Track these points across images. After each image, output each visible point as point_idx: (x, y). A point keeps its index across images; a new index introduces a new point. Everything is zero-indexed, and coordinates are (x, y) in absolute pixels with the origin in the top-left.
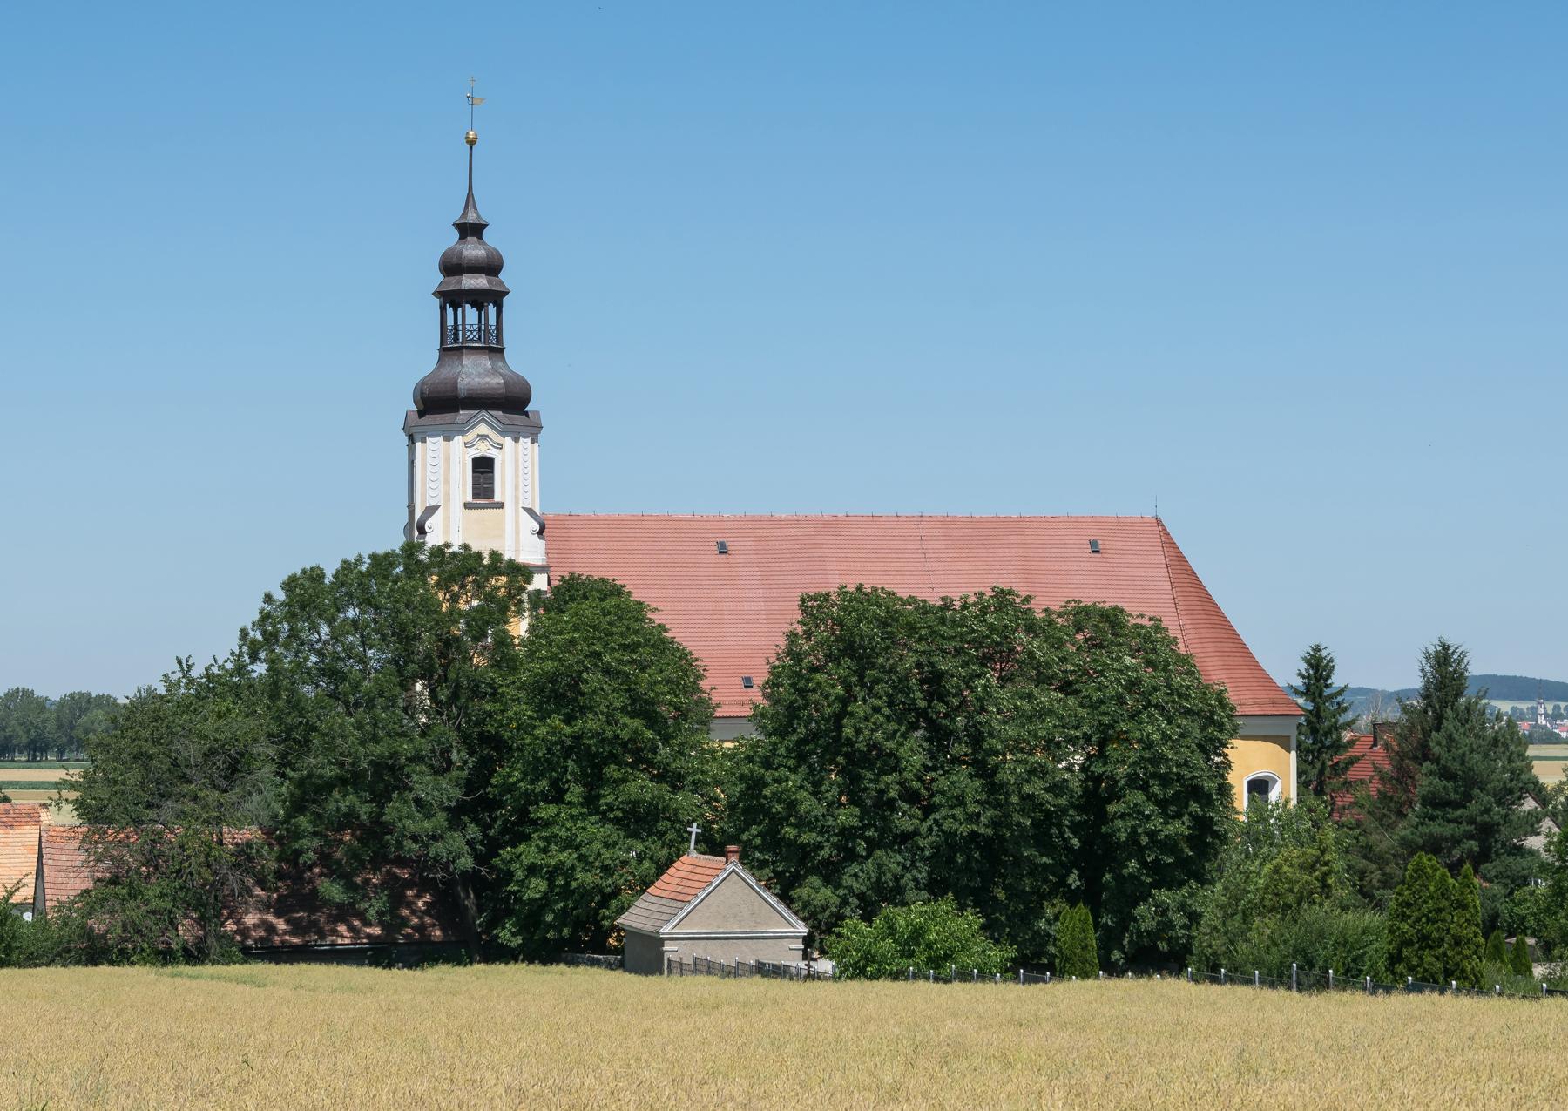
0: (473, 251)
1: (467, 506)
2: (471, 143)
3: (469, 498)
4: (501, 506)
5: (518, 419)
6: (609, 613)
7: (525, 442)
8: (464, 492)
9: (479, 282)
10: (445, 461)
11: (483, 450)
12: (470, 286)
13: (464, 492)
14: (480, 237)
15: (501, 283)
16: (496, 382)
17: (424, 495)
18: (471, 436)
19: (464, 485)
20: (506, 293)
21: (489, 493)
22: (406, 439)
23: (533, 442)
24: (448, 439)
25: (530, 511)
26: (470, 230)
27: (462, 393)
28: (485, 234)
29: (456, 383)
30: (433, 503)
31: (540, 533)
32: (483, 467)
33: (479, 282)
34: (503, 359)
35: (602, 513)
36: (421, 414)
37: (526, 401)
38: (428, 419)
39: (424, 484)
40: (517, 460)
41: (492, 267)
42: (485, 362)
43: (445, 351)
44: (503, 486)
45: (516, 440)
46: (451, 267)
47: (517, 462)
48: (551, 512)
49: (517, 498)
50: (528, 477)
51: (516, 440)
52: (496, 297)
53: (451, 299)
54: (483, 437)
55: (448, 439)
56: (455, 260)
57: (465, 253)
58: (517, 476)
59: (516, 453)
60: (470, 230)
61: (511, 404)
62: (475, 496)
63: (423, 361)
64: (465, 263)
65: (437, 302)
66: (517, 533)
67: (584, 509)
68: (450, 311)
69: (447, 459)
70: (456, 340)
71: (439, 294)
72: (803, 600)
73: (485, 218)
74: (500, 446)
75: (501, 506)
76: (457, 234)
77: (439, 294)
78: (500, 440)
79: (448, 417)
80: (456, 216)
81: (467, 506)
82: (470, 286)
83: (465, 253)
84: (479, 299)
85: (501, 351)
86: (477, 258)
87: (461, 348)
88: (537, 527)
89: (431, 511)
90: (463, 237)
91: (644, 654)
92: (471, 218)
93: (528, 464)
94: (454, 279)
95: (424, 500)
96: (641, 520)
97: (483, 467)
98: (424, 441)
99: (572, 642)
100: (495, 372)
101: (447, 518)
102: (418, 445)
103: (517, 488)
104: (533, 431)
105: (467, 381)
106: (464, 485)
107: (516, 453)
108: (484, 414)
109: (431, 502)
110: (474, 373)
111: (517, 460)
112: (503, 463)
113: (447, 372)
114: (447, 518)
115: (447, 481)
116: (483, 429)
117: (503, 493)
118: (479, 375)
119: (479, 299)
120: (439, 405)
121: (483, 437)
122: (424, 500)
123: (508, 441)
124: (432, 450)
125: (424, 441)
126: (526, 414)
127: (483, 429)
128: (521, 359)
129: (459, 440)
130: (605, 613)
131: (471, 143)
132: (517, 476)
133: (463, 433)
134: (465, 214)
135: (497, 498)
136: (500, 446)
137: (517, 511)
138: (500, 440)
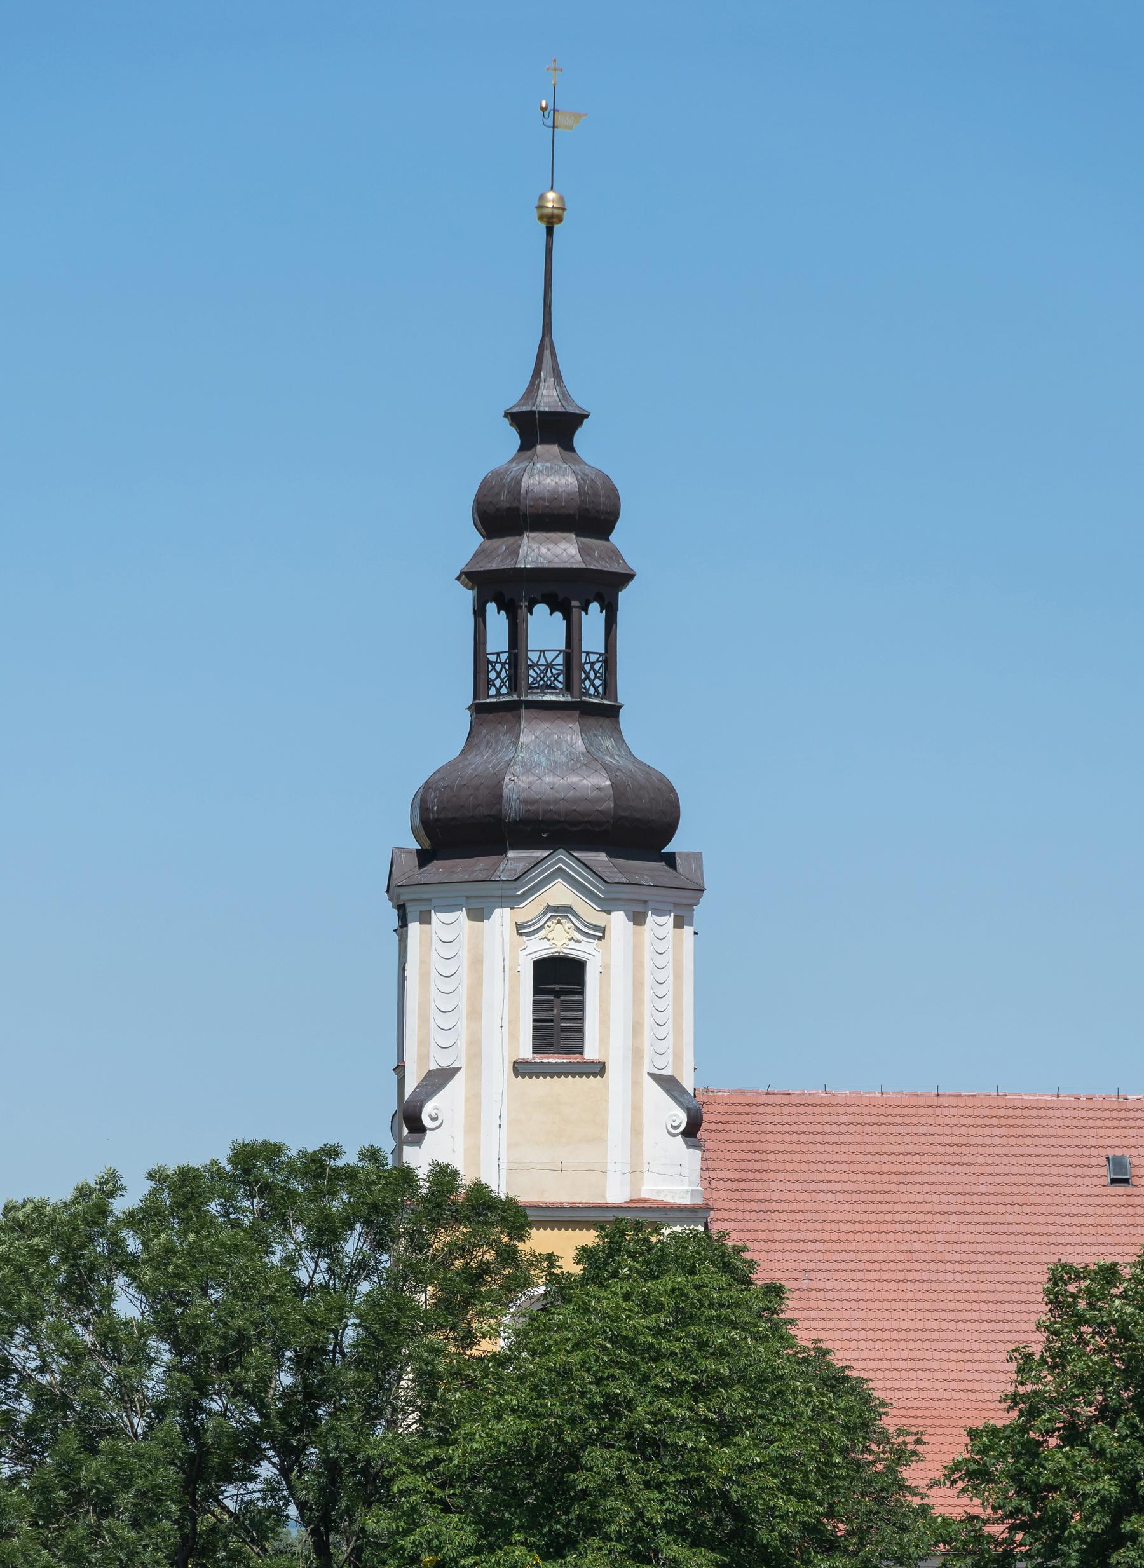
0: (549, 477)
1: (521, 1069)
2: (551, 221)
3: (526, 1052)
4: (598, 1069)
5: (646, 870)
6: (660, 1307)
7: (659, 925)
8: (514, 1036)
9: (559, 551)
10: (472, 966)
11: (558, 940)
12: (545, 560)
13: (514, 1036)
14: (567, 445)
15: (616, 554)
16: (593, 783)
17: (424, 1043)
18: (531, 909)
19: (514, 1022)
20: (627, 578)
21: (573, 1042)
22: (392, 917)
23: (679, 923)
24: (478, 915)
25: (669, 1084)
26: (547, 428)
27: (512, 810)
28: (580, 438)
29: (499, 785)
30: (446, 1062)
31: (691, 1132)
32: (559, 979)
33: (559, 551)
34: (617, 729)
35: (843, 1091)
36: (424, 857)
37: (669, 829)
38: (438, 869)
39: (424, 1020)
40: (638, 965)
41: (593, 516)
42: (571, 737)
43: (483, 711)
44: (607, 1017)
45: (638, 919)
46: (500, 515)
47: (637, 968)
48: (726, 1082)
49: (637, 1054)
50: (667, 1004)
51: (638, 919)
52: (604, 587)
53: (500, 589)
54: (559, 912)
55: (478, 915)
56: (504, 500)
57: (527, 482)
58: (638, 1001)
59: (637, 949)
60: (547, 428)
61: (632, 836)
62: (541, 1044)
63: (434, 734)
64: (526, 505)
65: (468, 596)
66: (637, 1132)
67: (801, 1078)
68: (497, 621)
69: (477, 962)
70: (514, 687)
71: (471, 578)
72: (1055, 1280)
73: (581, 400)
74: (600, 933)
75: (598, 1069)
76: (513, 438)
77: (471, 578)
78: (599, 919)
79: (480, 865)
80: (512, 397)
81: (521, 1069)
82: (545, 560)
83: (527, 482)
84: (568, 591)
85: (612, 712)
86: (555, 496)
87: (512, 708)
88: (682, 1118)
89: (438, 1079)
90: (527, 445)
91: (733, 1402)
92: (548, 399)
93: (668, 974)
94: (501, 544)
95: (423, 1057)
96: (931, 1108)
97: (559, 979)
98: (425, 919)
99: (565, 1374)
100: (592, 760)
101: (474, 1099)
102: (414, 928)
103: (637, 1029)
104: (682, 898)
105: (523, 781)
106: (514, 1022)
107: (637, 949)
108: (562, 859)
109: (439, 1060)
110: (547, 764)
111: (638, 965)
112: (605, 972)
113: (483, 761)
114: (474, 1099)
115: (475, 1013)
116: (559, 893)
117: (604, 1040)
118: (554, 768)
119: (568, 591)
120: (466, 837)
121: (559, 912)
122: (423, 1057)
123: (618, 921)
124: (444, 933)
125: (425, 919)
126: (671, 860)
127: (559, 893)
128: (656, 732)
129: (502, 918)
130: (649, 1306)
131: (551, 221)
132: (638, 1001)
133: (513, 901)
134: (532, 389)
135: (591, 1052)
136: (600, 933)
137: (636, 1084)
138: (599, 919)
